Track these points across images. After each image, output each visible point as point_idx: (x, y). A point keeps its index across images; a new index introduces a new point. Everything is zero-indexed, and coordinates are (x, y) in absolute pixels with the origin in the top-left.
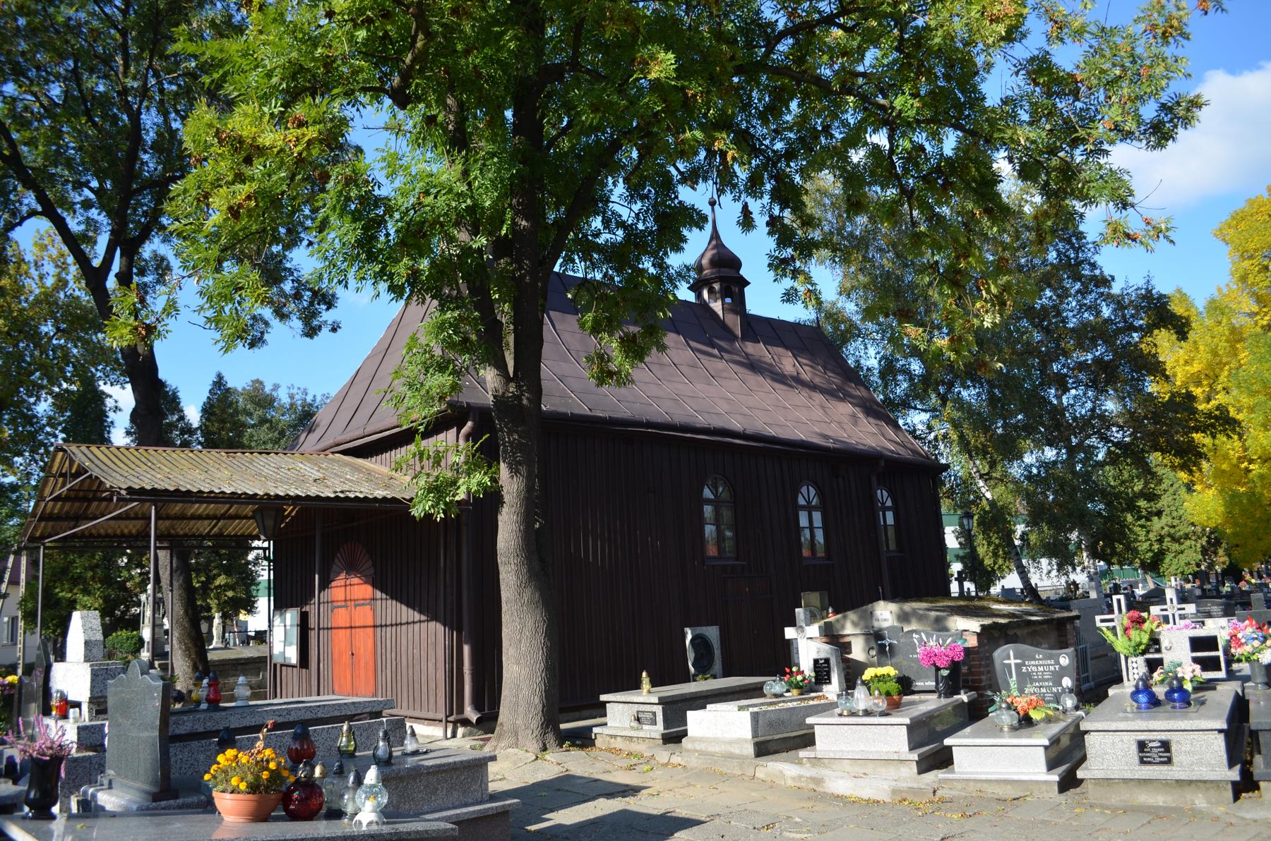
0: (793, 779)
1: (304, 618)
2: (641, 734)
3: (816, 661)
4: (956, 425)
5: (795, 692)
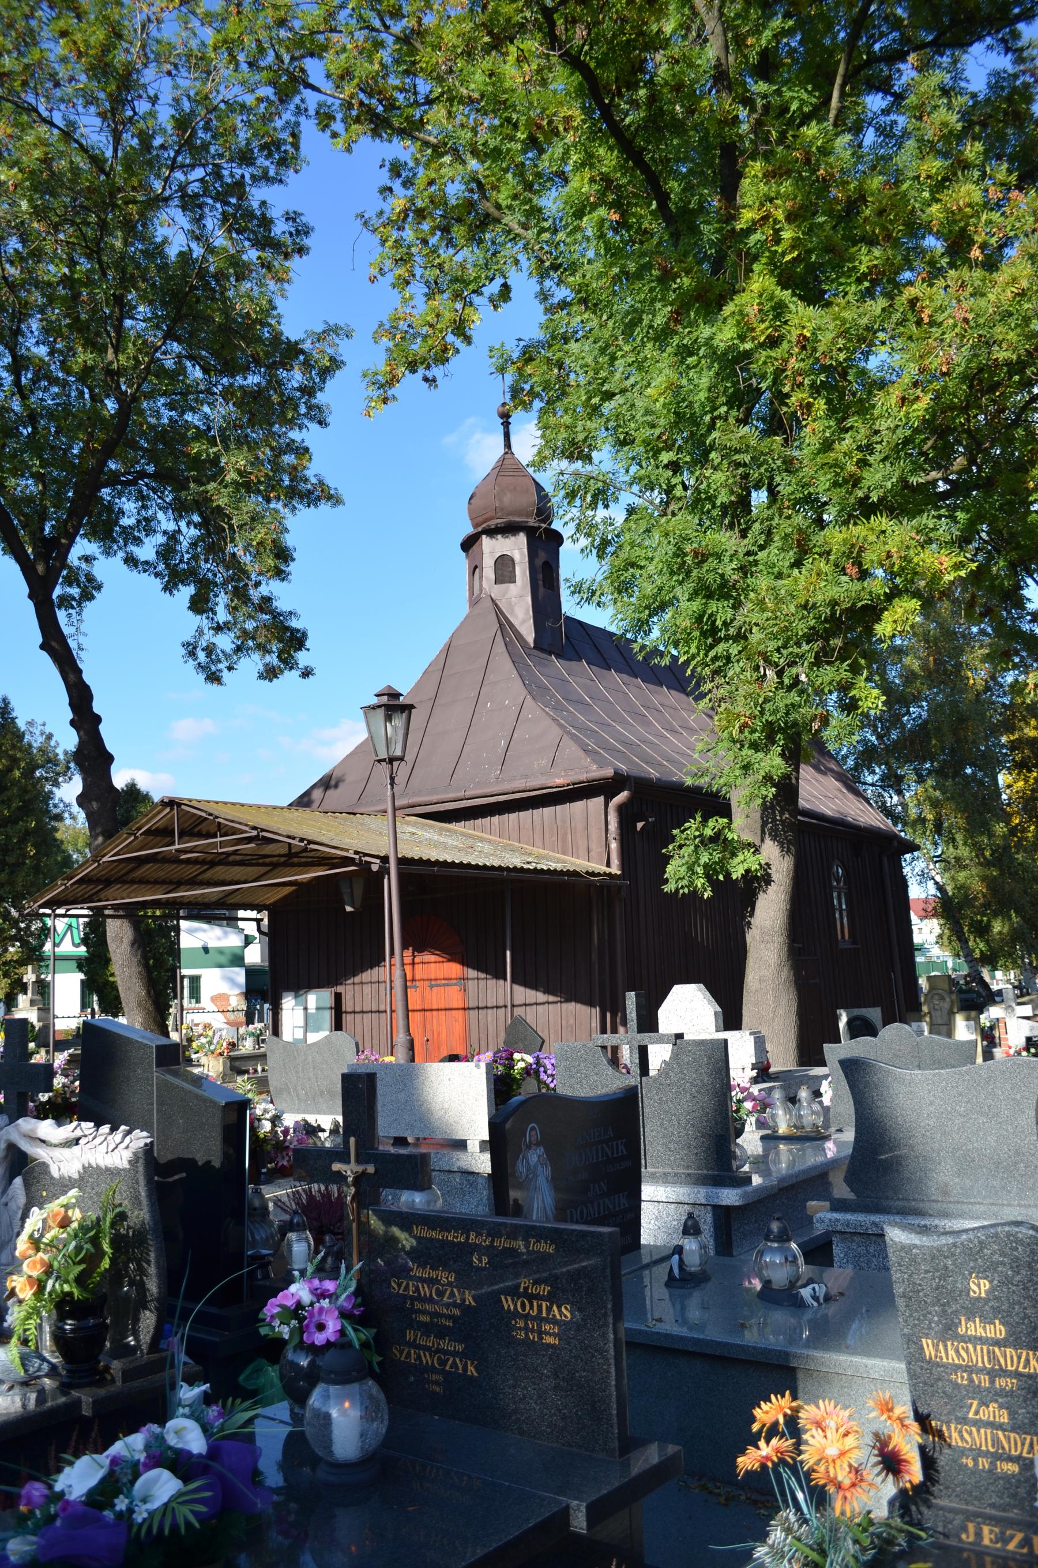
1: (338, 997)
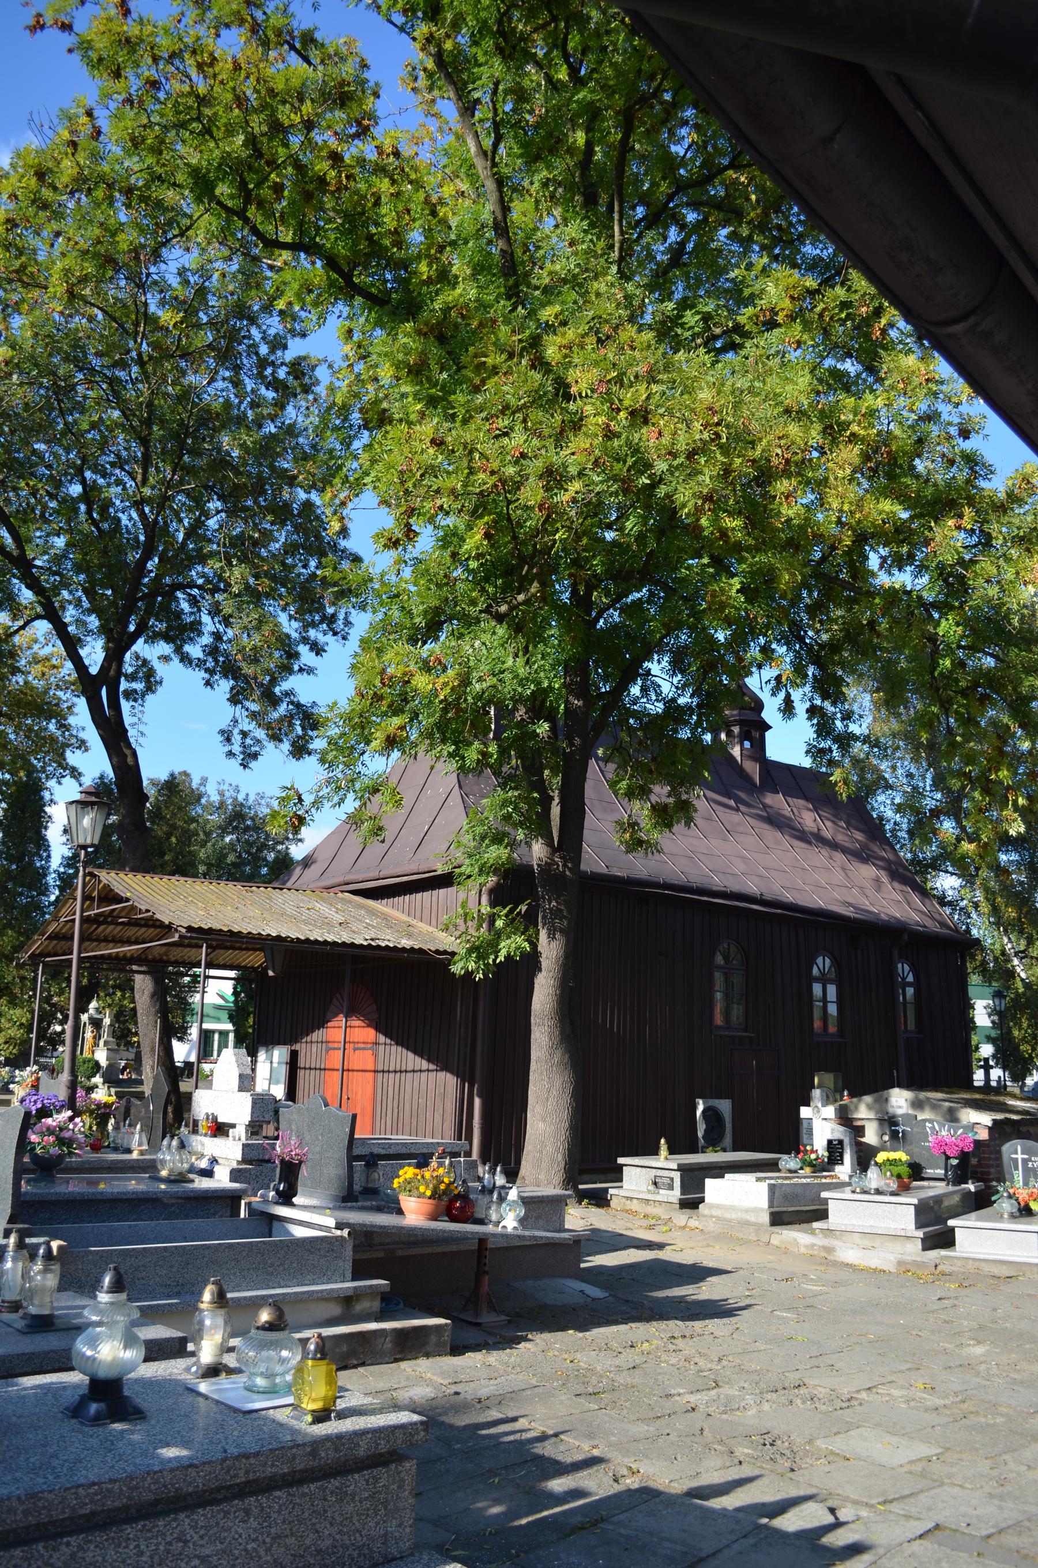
0: (806, 1246)
1: (294, 1055)
2: (658, 1198)
3: (830, 1142)
4: (990, 895)
5: (808, 1170)
